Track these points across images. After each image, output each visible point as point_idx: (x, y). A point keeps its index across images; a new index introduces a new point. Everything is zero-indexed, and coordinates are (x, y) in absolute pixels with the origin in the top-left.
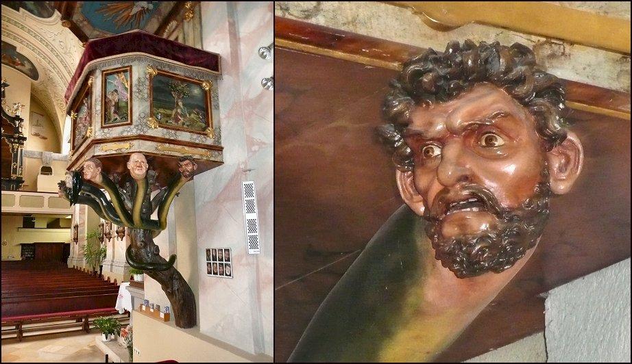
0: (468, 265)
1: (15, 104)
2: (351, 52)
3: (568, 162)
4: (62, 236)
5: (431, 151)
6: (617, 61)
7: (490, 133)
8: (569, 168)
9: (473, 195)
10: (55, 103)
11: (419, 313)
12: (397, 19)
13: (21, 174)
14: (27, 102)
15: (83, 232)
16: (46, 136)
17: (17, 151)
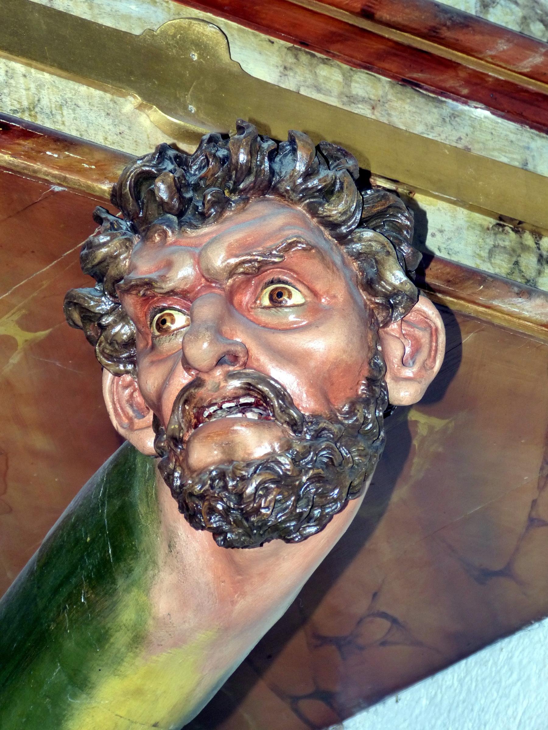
0: (237, 518)
5: (168, 319)
6: (488, 229)
7: (280, 281)
9: (249, 389)
11: (139, 639)
12: (108, 114)
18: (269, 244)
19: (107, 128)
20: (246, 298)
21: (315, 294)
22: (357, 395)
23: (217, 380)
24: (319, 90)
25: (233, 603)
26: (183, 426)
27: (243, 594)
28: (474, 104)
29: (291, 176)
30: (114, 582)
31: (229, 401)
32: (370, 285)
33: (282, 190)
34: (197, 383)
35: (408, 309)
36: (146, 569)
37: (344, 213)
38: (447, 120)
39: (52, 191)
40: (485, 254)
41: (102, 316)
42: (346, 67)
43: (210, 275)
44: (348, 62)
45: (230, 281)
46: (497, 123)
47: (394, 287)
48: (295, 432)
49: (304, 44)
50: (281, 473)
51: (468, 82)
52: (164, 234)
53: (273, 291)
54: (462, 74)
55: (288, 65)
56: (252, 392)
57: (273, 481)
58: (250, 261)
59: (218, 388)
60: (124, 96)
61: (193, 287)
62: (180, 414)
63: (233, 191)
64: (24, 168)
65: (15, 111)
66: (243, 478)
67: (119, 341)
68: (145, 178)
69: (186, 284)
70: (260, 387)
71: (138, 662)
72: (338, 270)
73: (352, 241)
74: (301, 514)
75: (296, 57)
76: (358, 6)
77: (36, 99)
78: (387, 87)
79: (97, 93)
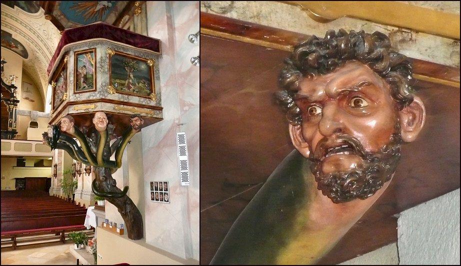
0: (342, 194)
1: (11, 76)
2: (256, 38)
3: (414, 118)
4: (45, 172)
5: (314, 110)
6: (450, 44)
7: (357, 97)
8: (415, 123)
9: (345, 142)
10: (40, 76)
11: (306, 228)
12: (290, 14)
13: (15, 127)
14: (19, 74)
15: (60, 169)
16: (34, 100)
17: (12, 111)
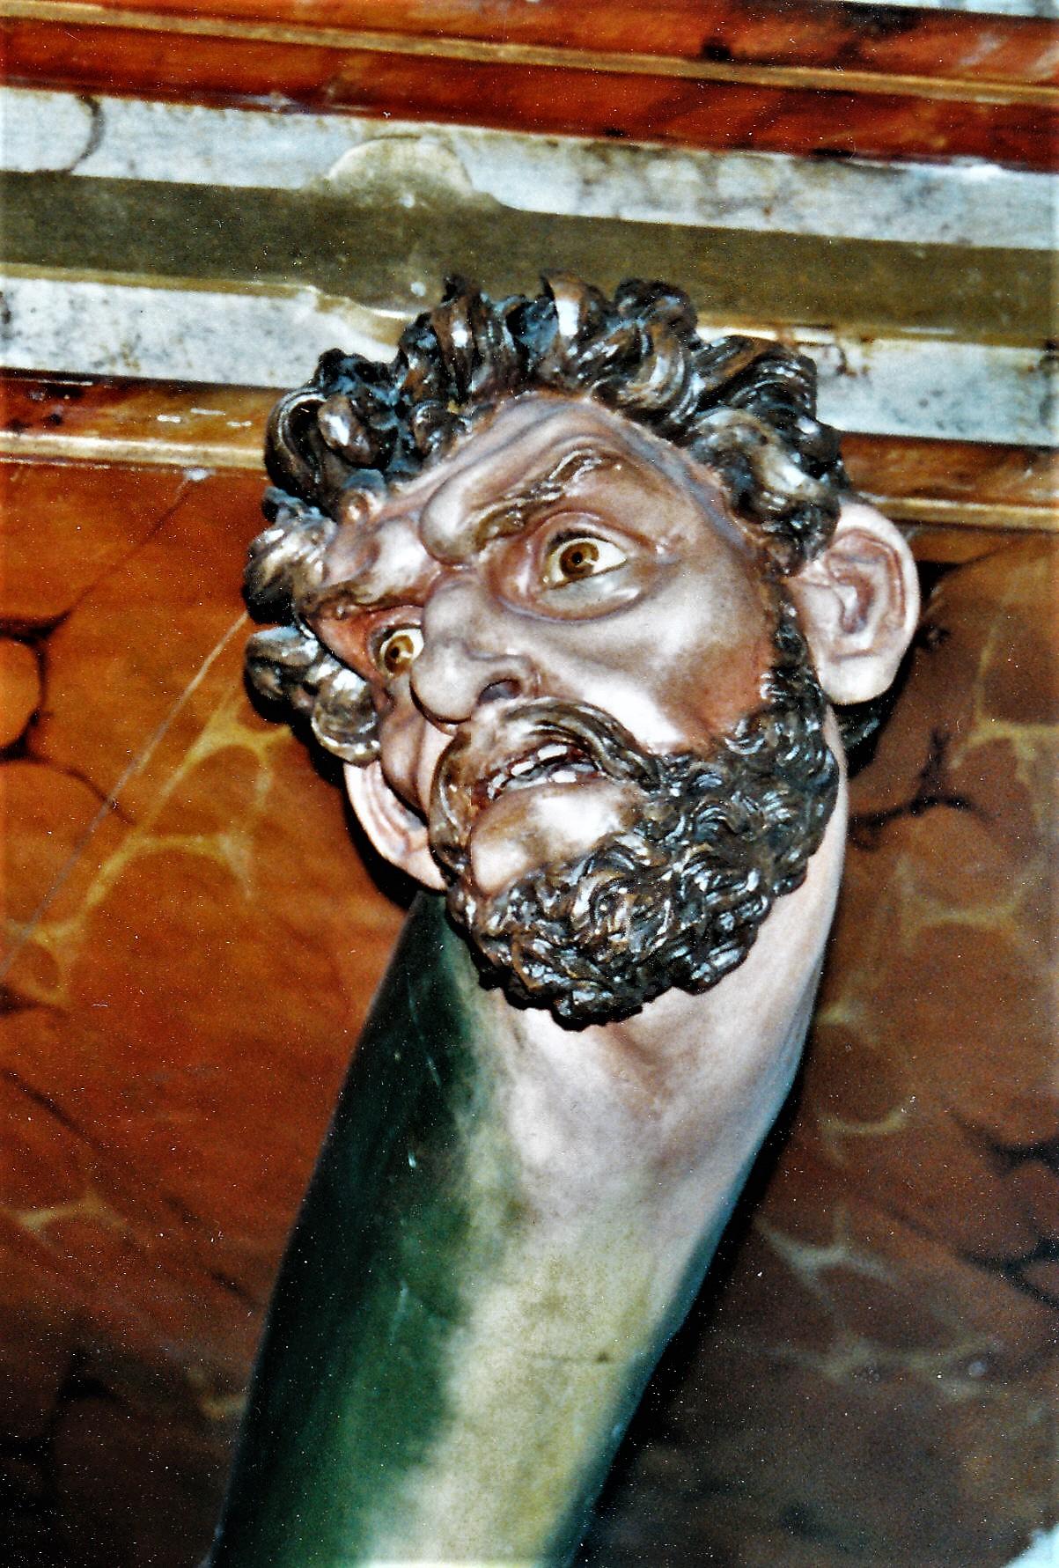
2: (126, 431)
3: (867, 595)
5: (401, 645)
8: (875, 614)
11: (517, 1212)
18: (534, 473)
19: (271, 355)
20: (522, 580)
21: (642, 541)
22: (760, 700)
23: (489, 729)
24: (654, 203)
25: (657, 1116)
26: (454, 821)
27: (669, 1095)
28: (963, 160)
29: (555, 350)
30: (451, 1120)
31: (519, 761)
32: (746, 504)
33: (547, 377)
34: (459, 743)
35: (829, 531)
36: (492, 1087)
37: (663, 389)
38: (916, 200)
39: (191, 482)
40: (1032, 414)
41: (307, 667)
42: (703, 154)
43: (444, 552)
44: (703, 145)
45: (484, 556)
46: (1016, 184)
47: (789, 498)
48: (647, 788)
49: (613, 133)
50: (632, 867)
51: (941, 127)
52: (363, 505)
53: (564, 555)
54: (928, 114)
55: (590, 176)
56: (555, 737)
57: (624, 883)
58: (506, 511)
59: (493, 742)
60: (291, 295)
61: (423, 578)
62: (445, 804)
63: (463, 398)
64: (128, 454)
65: (98, 364)
66: (566, 889)
67: (348, 705)
68: (305, 418)
69: (408, 577)
70: (563, 723)
71: (530, 1249)
72: (677, 488)
73: (696, 435)
74: (691, 930)
75: (604, 159)
76: (694, 42)
77: (133, 336)
78: (788, 172)
79: (240, 303)
